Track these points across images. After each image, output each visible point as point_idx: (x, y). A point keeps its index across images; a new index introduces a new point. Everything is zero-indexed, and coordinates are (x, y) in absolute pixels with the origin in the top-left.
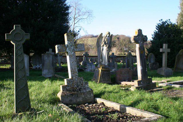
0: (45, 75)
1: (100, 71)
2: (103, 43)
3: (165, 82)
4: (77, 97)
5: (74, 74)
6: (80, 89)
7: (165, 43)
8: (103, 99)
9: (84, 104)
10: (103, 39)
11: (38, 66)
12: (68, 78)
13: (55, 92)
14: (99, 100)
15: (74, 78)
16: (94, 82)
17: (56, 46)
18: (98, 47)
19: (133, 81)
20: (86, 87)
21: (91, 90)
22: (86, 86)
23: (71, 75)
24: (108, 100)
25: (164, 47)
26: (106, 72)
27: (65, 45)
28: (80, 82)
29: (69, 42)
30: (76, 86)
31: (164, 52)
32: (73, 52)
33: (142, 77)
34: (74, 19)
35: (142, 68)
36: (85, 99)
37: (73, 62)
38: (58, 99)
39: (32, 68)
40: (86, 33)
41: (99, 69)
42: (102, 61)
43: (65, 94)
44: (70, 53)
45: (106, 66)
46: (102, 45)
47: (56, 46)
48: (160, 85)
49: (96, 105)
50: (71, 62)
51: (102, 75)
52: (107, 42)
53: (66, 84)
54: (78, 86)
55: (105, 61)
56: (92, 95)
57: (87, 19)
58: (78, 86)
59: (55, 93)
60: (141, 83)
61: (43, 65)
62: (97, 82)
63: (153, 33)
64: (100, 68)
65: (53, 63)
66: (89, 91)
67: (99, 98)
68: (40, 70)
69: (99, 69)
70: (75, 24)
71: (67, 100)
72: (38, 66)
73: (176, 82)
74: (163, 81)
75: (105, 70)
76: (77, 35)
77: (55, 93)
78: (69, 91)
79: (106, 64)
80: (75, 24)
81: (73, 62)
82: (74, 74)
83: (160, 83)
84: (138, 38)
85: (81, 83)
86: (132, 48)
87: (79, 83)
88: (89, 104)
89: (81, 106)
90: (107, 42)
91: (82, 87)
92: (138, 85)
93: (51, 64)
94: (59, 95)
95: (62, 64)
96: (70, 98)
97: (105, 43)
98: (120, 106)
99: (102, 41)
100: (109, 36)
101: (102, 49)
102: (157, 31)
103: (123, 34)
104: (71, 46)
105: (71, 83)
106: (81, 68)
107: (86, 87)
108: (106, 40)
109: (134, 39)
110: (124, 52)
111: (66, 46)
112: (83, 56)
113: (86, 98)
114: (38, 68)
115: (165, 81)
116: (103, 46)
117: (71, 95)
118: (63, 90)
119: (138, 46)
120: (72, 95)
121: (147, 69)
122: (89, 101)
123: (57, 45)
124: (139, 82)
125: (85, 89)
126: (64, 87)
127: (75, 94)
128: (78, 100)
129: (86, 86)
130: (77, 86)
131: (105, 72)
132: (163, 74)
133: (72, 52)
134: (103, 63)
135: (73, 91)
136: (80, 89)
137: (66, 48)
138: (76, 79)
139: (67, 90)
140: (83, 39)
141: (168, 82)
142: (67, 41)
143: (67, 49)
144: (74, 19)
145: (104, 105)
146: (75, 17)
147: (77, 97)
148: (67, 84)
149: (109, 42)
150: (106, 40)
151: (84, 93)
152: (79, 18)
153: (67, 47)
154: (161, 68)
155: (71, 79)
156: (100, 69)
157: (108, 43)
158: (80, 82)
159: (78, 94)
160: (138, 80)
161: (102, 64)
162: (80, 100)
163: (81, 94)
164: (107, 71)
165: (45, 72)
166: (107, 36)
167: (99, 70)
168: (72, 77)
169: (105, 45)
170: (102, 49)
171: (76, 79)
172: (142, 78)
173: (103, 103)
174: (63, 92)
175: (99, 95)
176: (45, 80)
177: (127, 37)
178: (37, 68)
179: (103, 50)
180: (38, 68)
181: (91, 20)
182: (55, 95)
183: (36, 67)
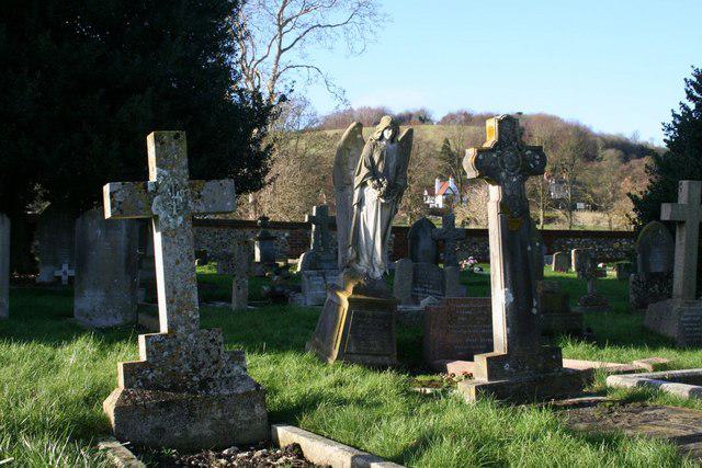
0: (87, 315)
1: (345, 305)
2: (365, 171)
3: (644, 370)
4: (191, 414)
5: (179, 312)
6: (204, 384)
7: (690, 177)
8: (308, 429)
9: (218, 450)
10: (366, 150)
11: (65, 267)
12: (157, 329)
13: (99, 391)
14: (286, 434)
15: (181, 330)
16: (308, 355)
17: (105, 188)
18: (342, 189)
19: (471, 359)
20: (233, 373)
21: (258, 389)
22: (236, 368)
23: (157, 308)
24: (326, 434)
25: (683, 198)
26: (375, 309)
27: (146, 187)
28: (207, 351)
29: (165, 172)
30: (186, 366)
31: (682, 223)
32: (181, 218)
33: (511, 338)
34: (281, 27)
35: (512, 300)
36: (229, 426)
37: (177, 263)
38: (106, 420)
39: (34, 280)
40: (338, 102)
41: (340, 294)
42: (358, 259)
43: (135, 403)
44: (166, 219)
45: (375, 281)
46: (357, 181)
47: (107, 189)
48: (612, 381)
49: (264, 456)
50: (172, 261)
51: (356, 323)
52: (380, 168)
53: (143, 357)
54: (196, 370)
55: (371, 258)
56: (258, 410)
57: (348, 26)
58: (196, 370)
59: (96, 395)
60: (507, 367)
61: (81, 263)
62: (323, 358)
63: (669, 120)
64: (343, 289)
65: (128, 259)
66: (247, 394)
67: (288, 428)
68: (66, 290)
69: (340, 294)
70: (281, 52)
71: (144, 429)
72: (65, 267)
73: (695, 370)
74: (637, 364)
75: (371, 302)
76: (276, 116)
77: (96, 395)
78: (155, 387)
79: (378, 274)
80: (281, 52)
81: (177, 263)
82: (179, 312)
83: (618, 373)
84: (496, 159)
85: (214, 353)
86: (594, 191)
87: (201, 357)
88: (242, 448)
89: (200, 458)
90: (380, 168)
91: (216, 371)
92: (490, 378)
93: (123, 263)
94: (109, 406)
95: (200, 264)
96: (154, 421)
97: (373, 173)
98: (353, 459)
99: (355, 163)
100: (392, 139)
101: (355, 201)
102: (692, 106)
103: (550, 111)
104: (175, 189)
105: (166, 353)
106: (279, 289)
107: (233, 373)
108: (376, 158)
109: (478, 163)
110: (545, 209)
111: (150, 188)
112: (308, 226)
113: (232, 421)
114: (65, 278)
115: (643, 366)
116: (363, 185)
117: (161, 405)
118: (127, 385)
119: (495, 192)
120: (167, 405)
121: (535, 303)
122: (245, 437)
123: (108, 185)
124: (495, 365)
125: (229, 382)
126: (131, 370)
127: (179, 403)
128: (194, 431)
129: (236, 368)
130: (193, 367)
131: (370, 313)
132: (671, 330)
133: (174, 217)
134: (363, 266)
135: (174, 388)
136: (204, 384)
137: (151, 200)
138: (191, 336)
139: (146, 385)
140: (331, 133)
141: (656, 368)
142: (155, 169)
143: (155, 200)
144: (281, 27)
145: (301, 455)
146: (286, 14)
147: (191, 414)
148: (148, 357)
149: (391, 165)
150: (376, 158)
151: (222, 401)
152: (306, 18)
153: (155, 193)
154: (669, 301)
155: (165, 335)
156: (344, 298)
157: (386, 173)
158: (207, 351)
159: (194, 402)
160: (489, 355)
161: (355, 270)
162: (202, 428)
163: (210, 405)
164: (381, 306)
165: (88, 301)
166: (382, 137)
167: (338, 297)
168: (172, 326)
169: (373, 180)
170: (355, 201)
171: (191, 336)
172: (509, 348)
173: (296, 446)
174: (124, 393)
175: (289, 416)
176: (381, 368)
177: (568, 127)
178: (59, 278)
179: (361, 203)
180: (65, 278)
181: (368, 35)
182: (91, 406)
183: (58, 273)
